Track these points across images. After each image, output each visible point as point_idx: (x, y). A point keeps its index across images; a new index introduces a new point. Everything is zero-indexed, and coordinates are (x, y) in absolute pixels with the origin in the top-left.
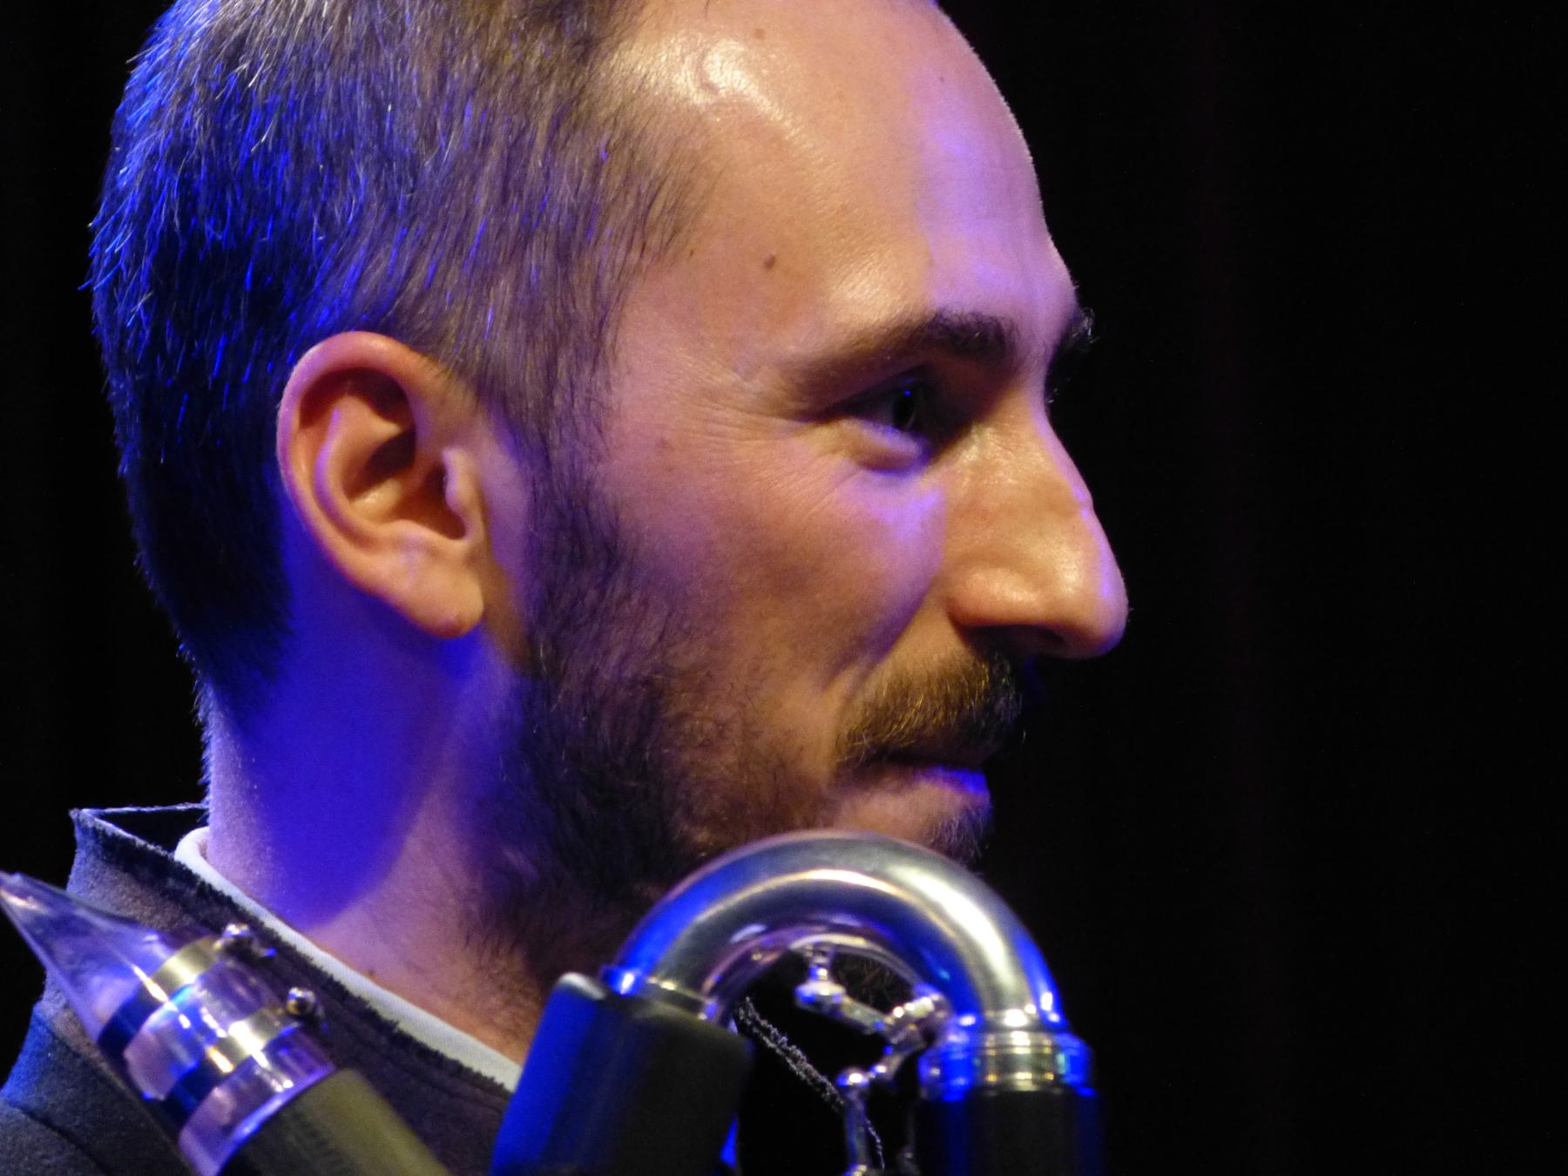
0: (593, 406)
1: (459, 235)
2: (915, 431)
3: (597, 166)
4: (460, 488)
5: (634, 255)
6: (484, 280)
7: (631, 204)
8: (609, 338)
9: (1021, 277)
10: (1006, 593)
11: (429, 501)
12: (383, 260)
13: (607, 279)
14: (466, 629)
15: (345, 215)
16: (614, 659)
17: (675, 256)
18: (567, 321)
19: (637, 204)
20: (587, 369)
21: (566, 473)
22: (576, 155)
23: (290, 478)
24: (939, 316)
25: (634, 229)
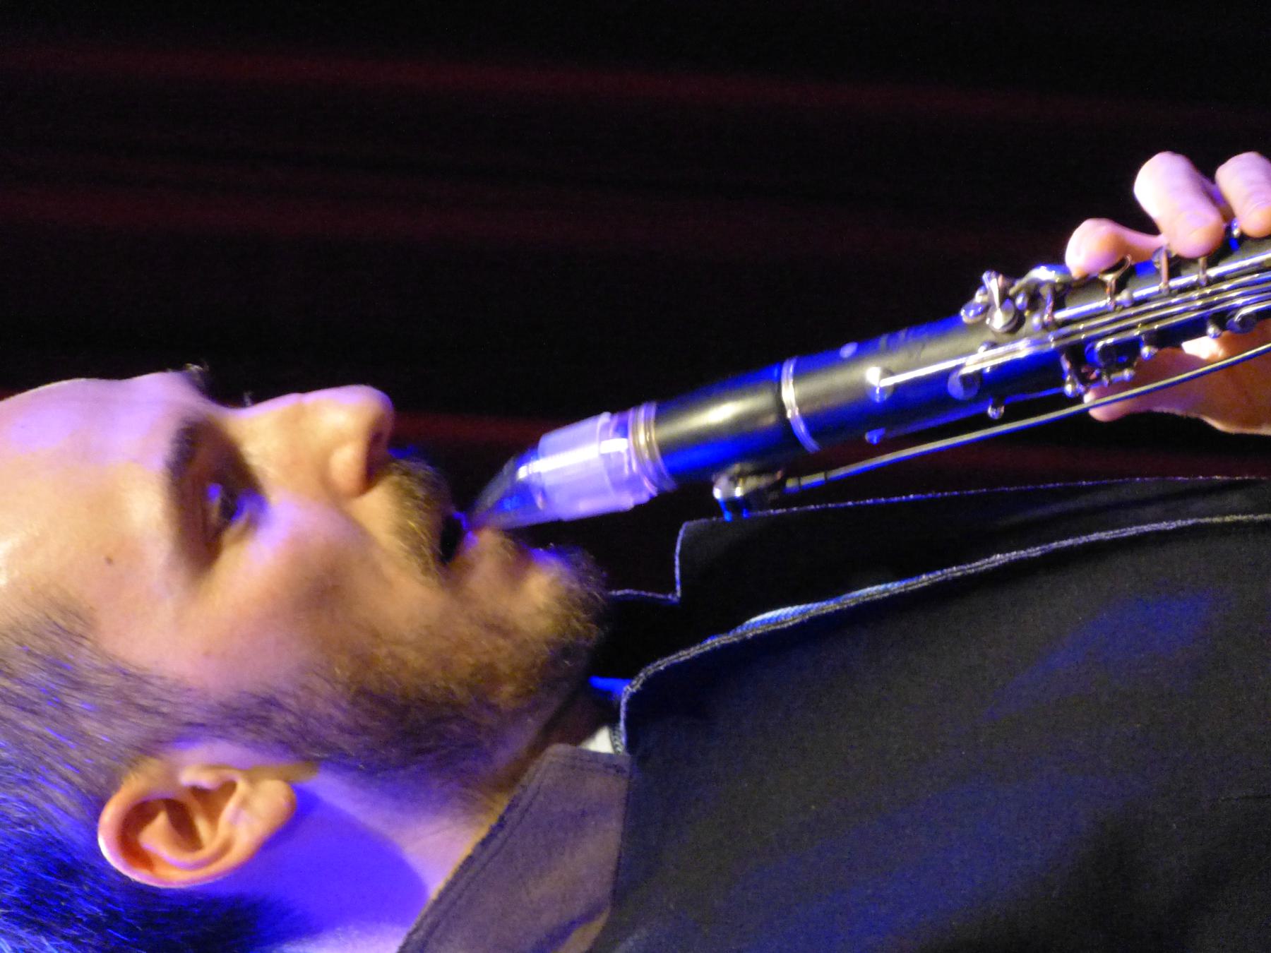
1: (51, 745)
3: (29, 653)
4: (206, 780)
6: (82, 737)
7: (56, 638)
8: (132, 670)
10: (347, 461)
11: (210, 799)
12: (59, 796)
13: (98, 663)
14: (294, 796)
15: (23, 811)
18: (118, 693)
19: (57, 635)
22: (20, 664)
23: (179, 883)
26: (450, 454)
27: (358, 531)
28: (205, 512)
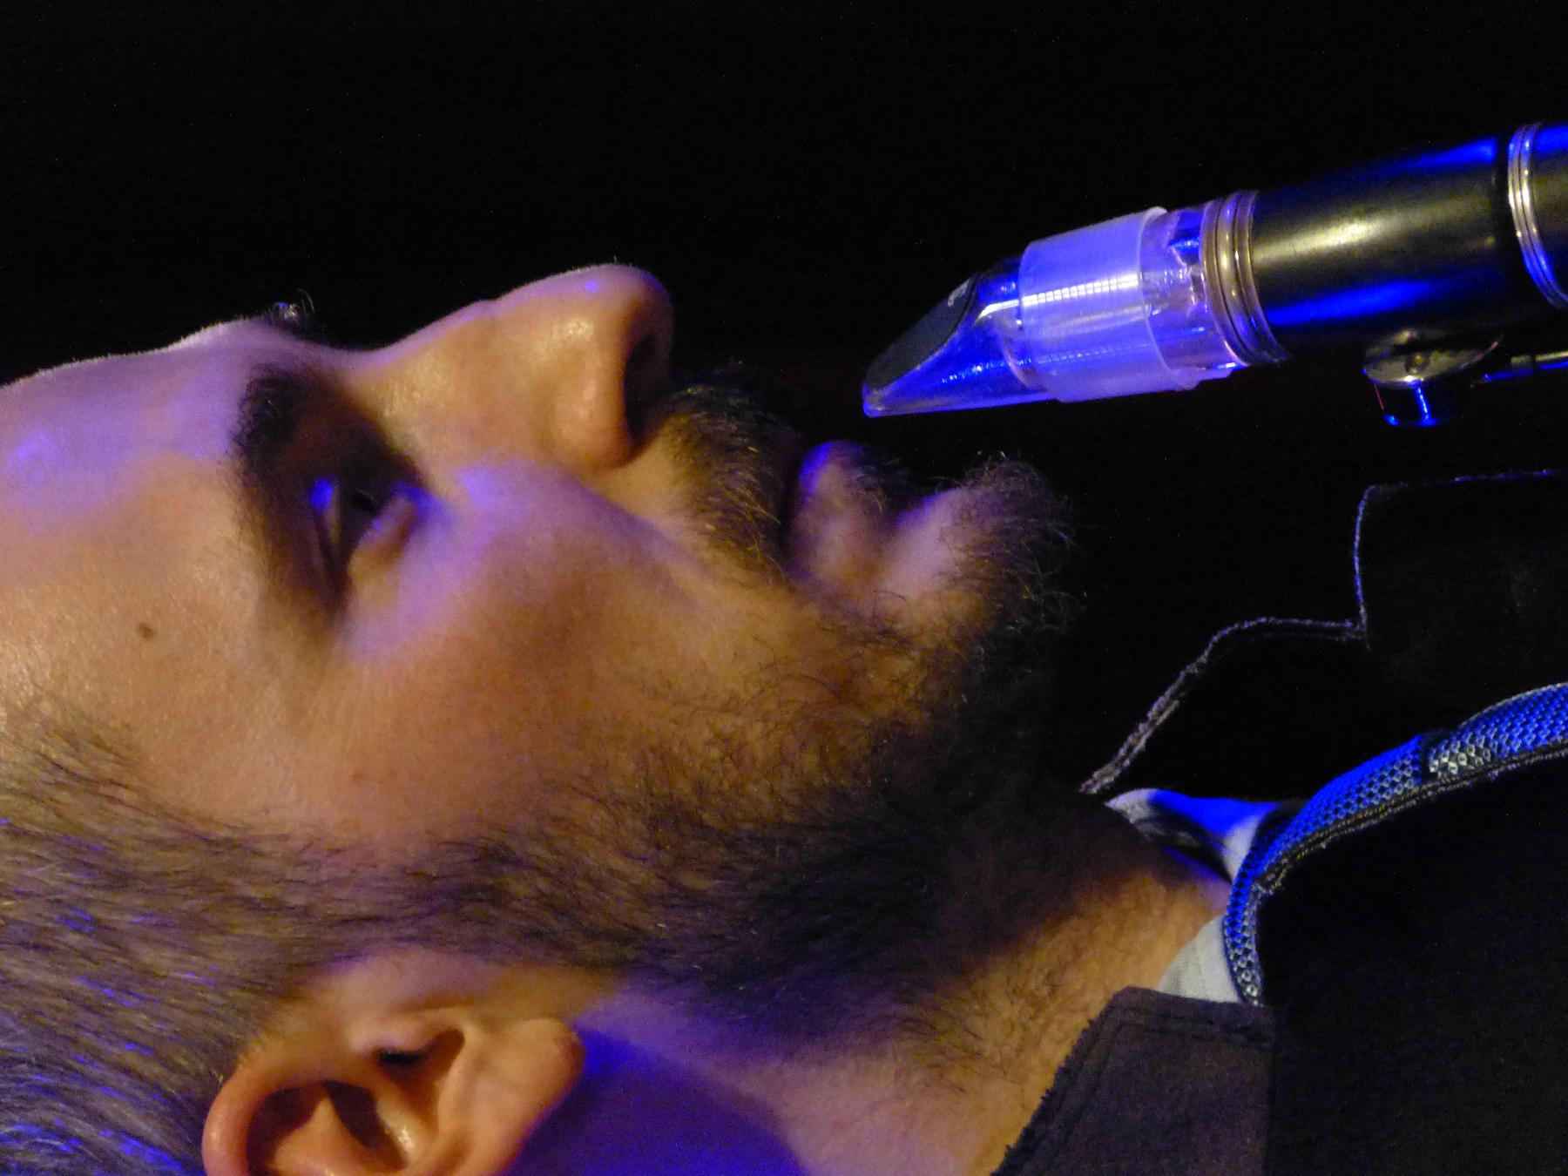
0: (306, 856)
2: (385, 497)
4: (401, 1034)
5: (124, 794)
7: (64, 796)
8: (224, 833)
9: (213, 361)
10: (587, 407)
11: (412, 1070)
15: (57, 1153)
16: (618, 864)
17: (129, 748)
18: (199, 883)
20: (261, 863)
21: (390, 897)
24: (236, 439)
25: (95, 794)
26: (778, 359)
27: (626, 525)
28: (321, 528)
